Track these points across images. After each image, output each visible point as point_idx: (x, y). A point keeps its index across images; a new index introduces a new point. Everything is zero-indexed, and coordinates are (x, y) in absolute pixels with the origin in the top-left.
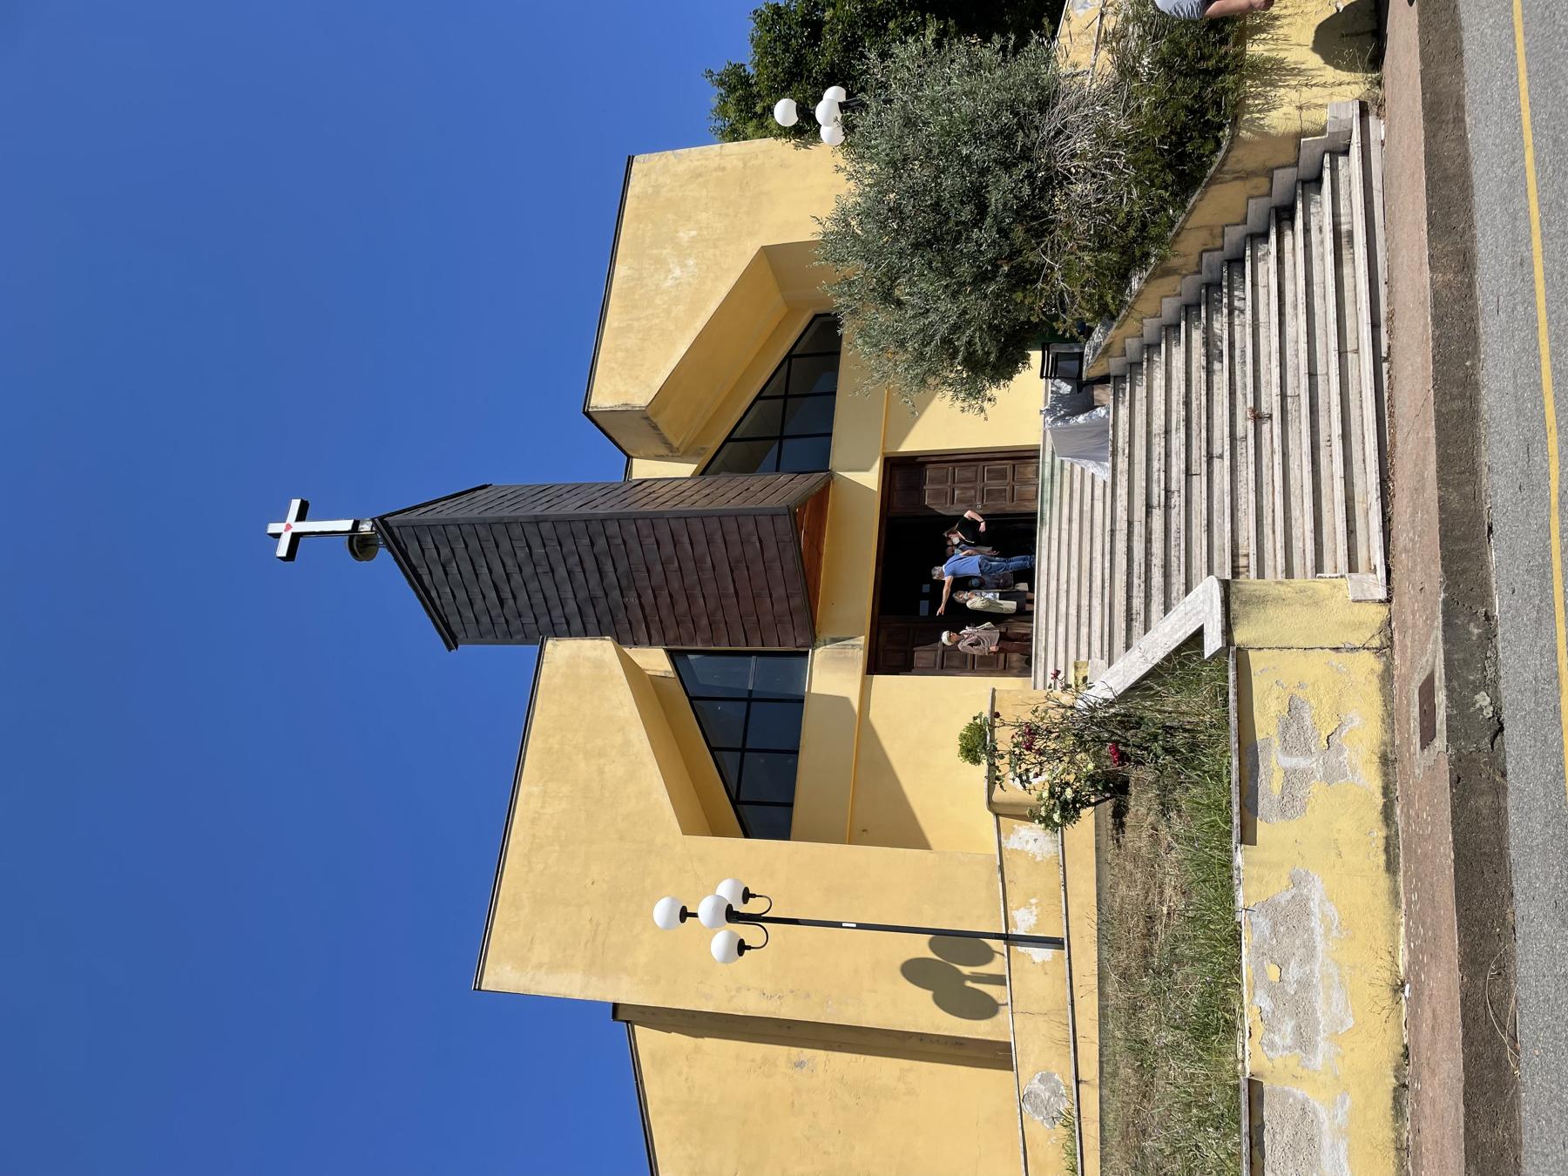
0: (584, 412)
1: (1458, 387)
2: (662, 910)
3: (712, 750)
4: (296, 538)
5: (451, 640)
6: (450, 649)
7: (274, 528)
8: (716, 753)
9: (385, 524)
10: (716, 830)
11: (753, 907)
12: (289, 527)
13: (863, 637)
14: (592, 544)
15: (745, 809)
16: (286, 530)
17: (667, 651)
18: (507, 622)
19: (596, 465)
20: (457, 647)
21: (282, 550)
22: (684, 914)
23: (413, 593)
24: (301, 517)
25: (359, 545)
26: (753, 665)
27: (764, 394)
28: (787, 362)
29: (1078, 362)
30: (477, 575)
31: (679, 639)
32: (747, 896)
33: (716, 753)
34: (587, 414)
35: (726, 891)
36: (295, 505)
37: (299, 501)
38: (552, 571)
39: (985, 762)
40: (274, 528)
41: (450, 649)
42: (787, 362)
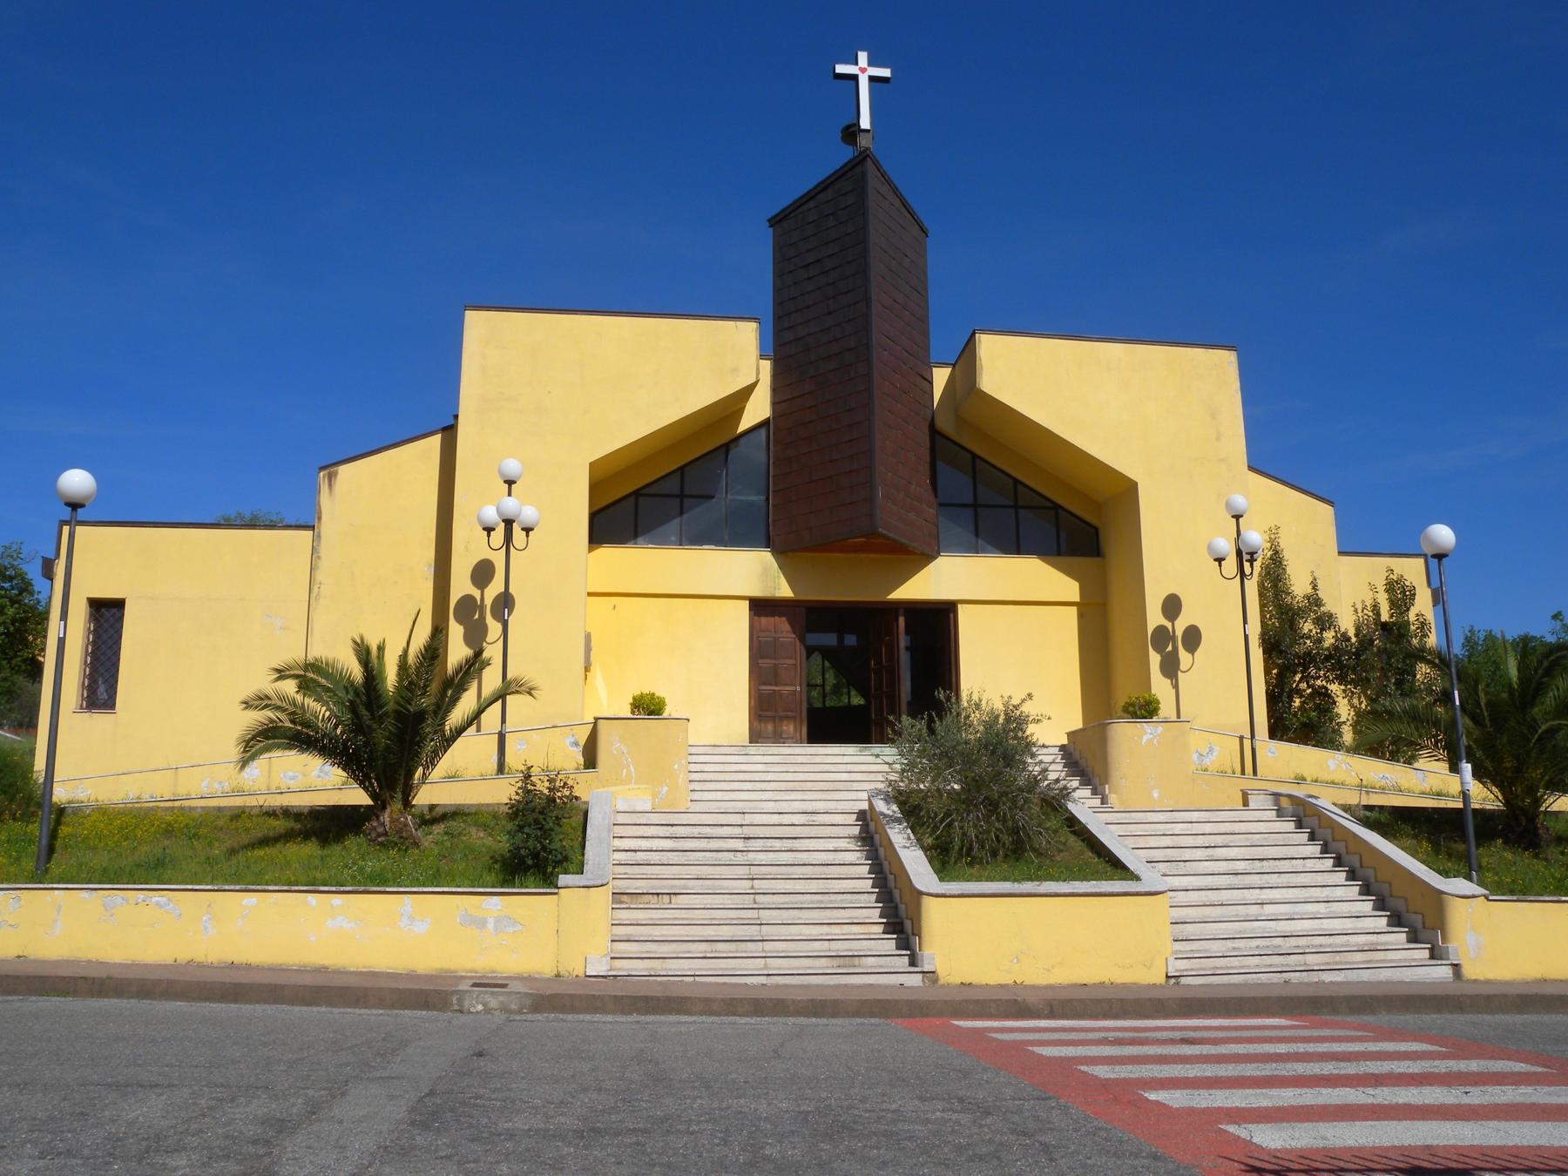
0: (975, 330)
1: (393, 849)
2: (512, 466)
3: (681, 469)
4: (855, 78)
5: (775, 222)
6: (769, 221)
7: (863, 57)
8: (679, 473)
9: (865, 158)
10: (595, 488)
11: (518, 534)
12: (863, 70)
13: (793, 596)
14: (849, 350)
15: (632, 499)
16: (860, 69)
17: (769, 418)
18: (790, 272)
19: (941, 339)
20: (770, 226)
21: (841, 69)
22: (510, 483)
23: (838, 167)
24: (872, 79)
25: (851, 132)
26: (755, 498)
27: (1019, 486)
28: (1051, 505)
29: (1281, 798)
30: (827, 243)
31: (777, 429)
32: (527, 530)
33: (724, 448)
34: (973, 334)
35: (528, 513)
36: (885, 72)
37: (889, 76)
38: (830, 313)
39: (447, 728)
40: (863, 57)
41: (769, 221)
42: (1051, 505)
